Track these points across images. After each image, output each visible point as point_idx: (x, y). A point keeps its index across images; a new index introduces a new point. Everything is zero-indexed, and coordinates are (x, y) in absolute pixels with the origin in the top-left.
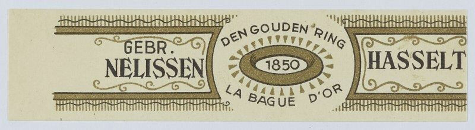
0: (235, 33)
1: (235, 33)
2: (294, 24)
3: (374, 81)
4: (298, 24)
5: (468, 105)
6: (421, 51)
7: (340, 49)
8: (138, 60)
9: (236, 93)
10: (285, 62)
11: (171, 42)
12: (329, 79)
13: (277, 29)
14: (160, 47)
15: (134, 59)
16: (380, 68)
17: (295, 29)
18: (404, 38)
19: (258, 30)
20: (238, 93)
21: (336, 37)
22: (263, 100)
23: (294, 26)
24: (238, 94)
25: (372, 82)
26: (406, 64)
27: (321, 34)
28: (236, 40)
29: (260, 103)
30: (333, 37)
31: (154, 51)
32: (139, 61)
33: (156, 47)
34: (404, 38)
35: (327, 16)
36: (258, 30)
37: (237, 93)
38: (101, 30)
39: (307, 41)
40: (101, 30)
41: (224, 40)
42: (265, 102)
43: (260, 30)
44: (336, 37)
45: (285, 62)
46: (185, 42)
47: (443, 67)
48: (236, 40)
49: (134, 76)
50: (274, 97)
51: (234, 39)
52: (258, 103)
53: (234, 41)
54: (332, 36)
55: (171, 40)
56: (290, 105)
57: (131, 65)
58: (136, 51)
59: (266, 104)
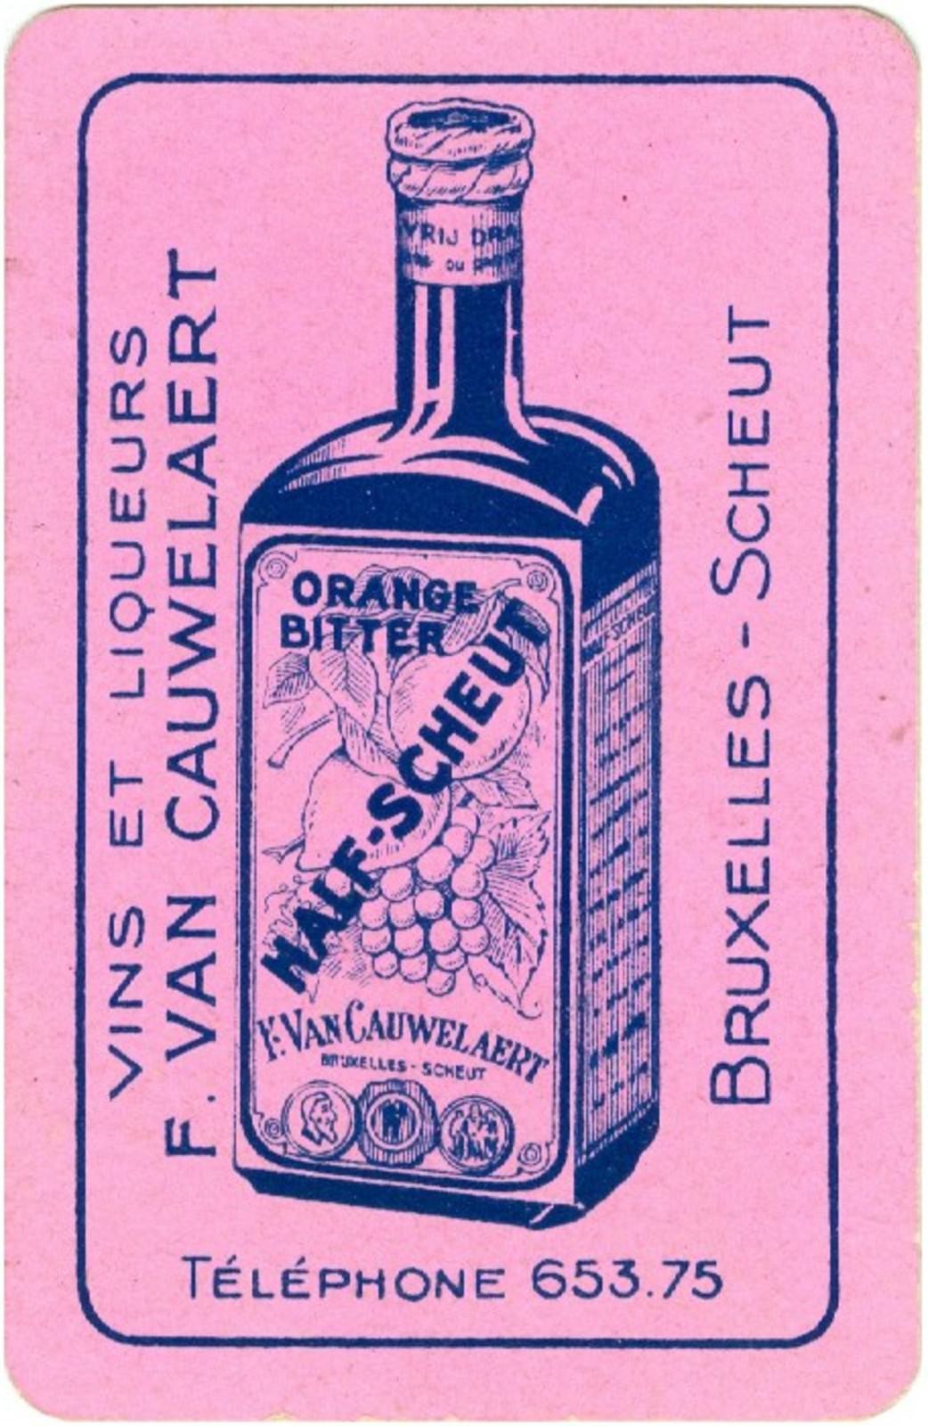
5: (774, 491)
6: (460, 611)
9: (198, 474)
10: (585, 1268)
16: (527, 421)
18: (466, 132)
22: (189, 763)
24: (200, 461)
26: (484, 708)
34: (466, 132)
39: (469, 675)
42: (199, 751)
45: (585, 1268)
46: (543, 1288)
47: (457, 1047)
50: (137, 492)
52: (212, 784)
53: (480, 1295)
57: (117, 913)
59: (212, 744)
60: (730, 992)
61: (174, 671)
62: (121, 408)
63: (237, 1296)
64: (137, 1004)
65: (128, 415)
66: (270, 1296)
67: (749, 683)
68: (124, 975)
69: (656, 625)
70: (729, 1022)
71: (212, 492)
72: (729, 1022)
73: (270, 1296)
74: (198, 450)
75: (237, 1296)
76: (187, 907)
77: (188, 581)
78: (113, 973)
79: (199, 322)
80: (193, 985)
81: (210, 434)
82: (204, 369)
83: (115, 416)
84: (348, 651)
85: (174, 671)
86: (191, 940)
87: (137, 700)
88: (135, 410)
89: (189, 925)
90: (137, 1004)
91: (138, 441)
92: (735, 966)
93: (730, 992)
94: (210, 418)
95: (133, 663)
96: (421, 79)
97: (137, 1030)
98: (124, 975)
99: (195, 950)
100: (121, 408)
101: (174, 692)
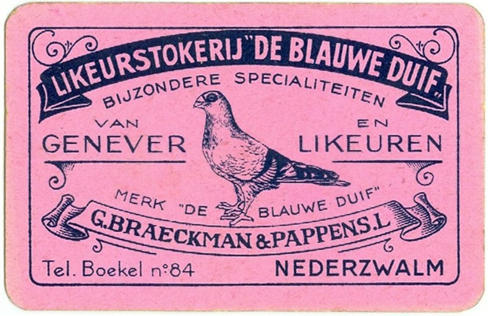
0: (372, 189)
1: (372, 189)
2: (329, 262)
3: (391, 251)
4: (336, 261)
9: (282, 213)
12: (143, 61)
13: (297, 211)
14: (392, 142)
15: (301, 230)
19: (58, 146)
23: (311, 38)
24: (403, 271)
25: (390, 249)
28: (266, 83)
31: (268, 215)
32: (318, 241)
36: (58, 146)
37: (401, 269)
38: (65, 67)
40: (65, 67)
43: (182, 271)
48: (266, 83)
54: (159, 86)
60: (219, 83)
61: (302, 205)
63: (191, 86)
64: (164, 83)
66: (422, 274)
67: (243, 78)
69: (311, 66)
70: (110, 106)
72: (110, 106)
73: (422, 274)
74: (286, 212)
75: (191, 86)
77: (319, 205)
79: (205, 82)
82: (341, 273)
85: (302, 205)
87: (198, 75)
90: (164, 83)
91: (130, 99)
93: (219, 83)
94: (349, 150)
96: (368, 66)
97: (75, 143)
101: (298, 205)
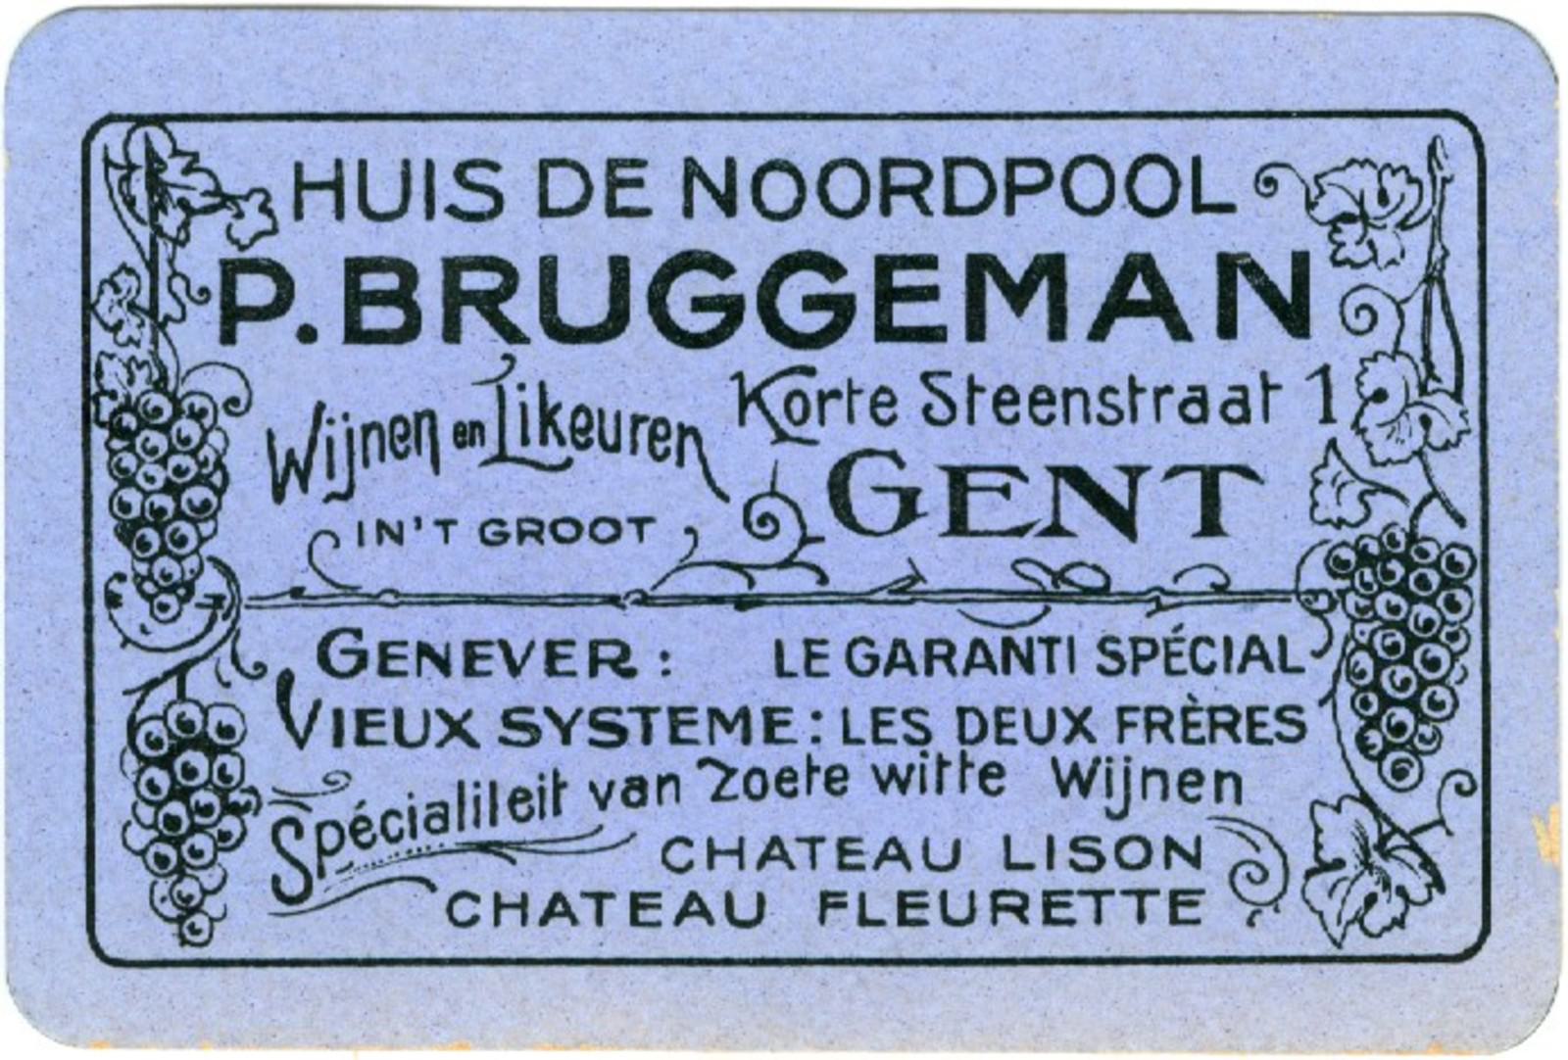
7: (1321, 416)
8: (917, 491)
9: (884, 856)
11: (1446, 504)
17: (393, 665)
20: (892, 851)
21: (730, 164)
27: (509, 288)
28: (627, 212)
29: (1143, 666)
30: (709, 195)
33: (429, 295)
35: (666, 673)
41: (553, 173)
44: (730, 164)
48: (627, 212)
49: (925, 581)
51: (905, 314)
52: (1135, 671)
55: (1442, 510)
56: (612, 210)
58: (233, 297)
62: (1002, 900)
65: (996, 908)
66: (880, 923)
68: (1174, 855)
71: (871, 651)
73: (880, 923)
76: (721, 187)
78: (127, 697)
80: (1146, 296)
81: (525, 330)
83: (995, 895)
84: (1368, 884)
86: (1171, 611)
88: (1001, 916)
89: (698, 187)
92: (1044, 842)
95: (1041, 862)
98: (1174, 855)
99: (1197, 301)
100: (1002, 900)
